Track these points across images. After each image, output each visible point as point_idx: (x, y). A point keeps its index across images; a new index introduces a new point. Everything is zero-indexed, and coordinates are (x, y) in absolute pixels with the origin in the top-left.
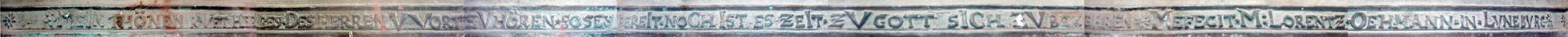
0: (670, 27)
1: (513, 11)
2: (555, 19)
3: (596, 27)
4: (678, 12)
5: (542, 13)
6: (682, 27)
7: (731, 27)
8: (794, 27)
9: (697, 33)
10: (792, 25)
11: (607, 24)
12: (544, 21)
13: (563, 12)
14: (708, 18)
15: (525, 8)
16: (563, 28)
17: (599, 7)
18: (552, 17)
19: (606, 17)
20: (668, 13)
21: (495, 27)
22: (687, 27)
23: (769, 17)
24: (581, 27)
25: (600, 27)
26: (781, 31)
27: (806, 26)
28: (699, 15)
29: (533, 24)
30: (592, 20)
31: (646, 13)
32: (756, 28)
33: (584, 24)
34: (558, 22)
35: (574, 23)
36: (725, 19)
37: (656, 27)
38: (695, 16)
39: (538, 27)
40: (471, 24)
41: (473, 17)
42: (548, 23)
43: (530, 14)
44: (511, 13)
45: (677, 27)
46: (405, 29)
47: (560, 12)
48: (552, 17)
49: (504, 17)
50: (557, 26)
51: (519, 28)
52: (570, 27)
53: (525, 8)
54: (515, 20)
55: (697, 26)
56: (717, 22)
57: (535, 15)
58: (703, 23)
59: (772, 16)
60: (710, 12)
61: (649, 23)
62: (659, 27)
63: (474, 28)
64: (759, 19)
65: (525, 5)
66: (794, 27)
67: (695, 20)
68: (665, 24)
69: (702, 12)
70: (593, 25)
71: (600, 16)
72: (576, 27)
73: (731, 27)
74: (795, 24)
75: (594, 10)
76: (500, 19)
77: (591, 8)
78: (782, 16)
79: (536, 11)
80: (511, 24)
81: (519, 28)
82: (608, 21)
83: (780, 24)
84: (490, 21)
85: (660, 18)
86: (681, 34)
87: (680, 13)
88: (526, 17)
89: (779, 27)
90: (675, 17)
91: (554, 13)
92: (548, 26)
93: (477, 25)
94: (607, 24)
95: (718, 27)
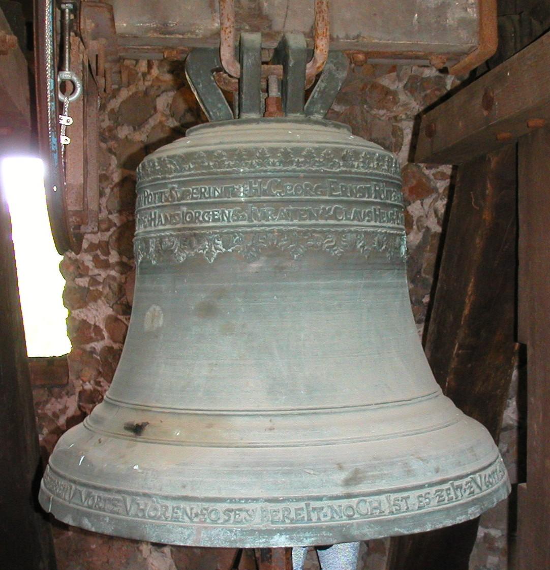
0: (337, 518)
1: (155, 500)
2: (194, 511)
3: (236, 522)
4: (342, 501)
5: (182, 504)
6: (350, 517)
7: (399, 511)
8: (446, 501)
9: (369, 522)
10: (444, 500)
11: (248, 518)
12: (183, 514)
13: (204, 504)
14: (376, 504)
15: (166, 498)
16: (201, 522)
17: (240, 499)
18: (192, 509)
19: (247, 511)
20: (330, 503)
21: (137, 515)
22: (356, 516)
23: (427, 496)
24: (220, 522)
25: (240, 522)
26: (439, 507)
27: (454, 497)
28: (365, 501)
29: (172, 515)
30: (232, 514)
31: (302, 504)
32: (420, 508)
33: (223, 517)
34: (197, 515)
35: (213, 516)
36: (392, 503)
37: (319, 519)
38: (362, 504)
39: (176, 519)
40: (115, 509)
41: (118, 500)
42: (187, 515)
43: (170, 504)
44: (153, 502)
45: (344, 518)
46: (74, 503)
47: (200, 504)
48: (192, 509)
49: (146, 505)
50: (196, 520)
51: (159, 518)
52: (208, 520)
53: (166, 498)
54: (155, 509)
55: (367, 514)
56: (385, 507)
57: (175, 505)
58: (372, 510)
59: (429, 493)
60: (376, 497)
61: (309, 516)
62: (323, 519)
63: (118, 514)
64: (420, 499)
65: (166, 494)
66: (446, 501)
67: (364, 508)
68: (329, 515)
69: (368, 499)
70: (232, 518)
71: (240, 510)
72: (214, 522)
73: (399, 511)
74: (447, 498)
75: (235, 502)
76: (142, 507)
77: (232, 501)
78: (437, 491)
79: (176, 502)
80: (152, 514)
81: (159, 518)
82: (250, 516)
83: (436, 501)
84: (132, 509)
85: (322, 509)
86: (352, 525)
87: (344, 502)
88: (167, 507)
89: (436, 504)
90: (340, 506)
91: (194, 505)
92: (186, 519)
93: (121, 510)
94: (248, 518)
95: (387, 512)
